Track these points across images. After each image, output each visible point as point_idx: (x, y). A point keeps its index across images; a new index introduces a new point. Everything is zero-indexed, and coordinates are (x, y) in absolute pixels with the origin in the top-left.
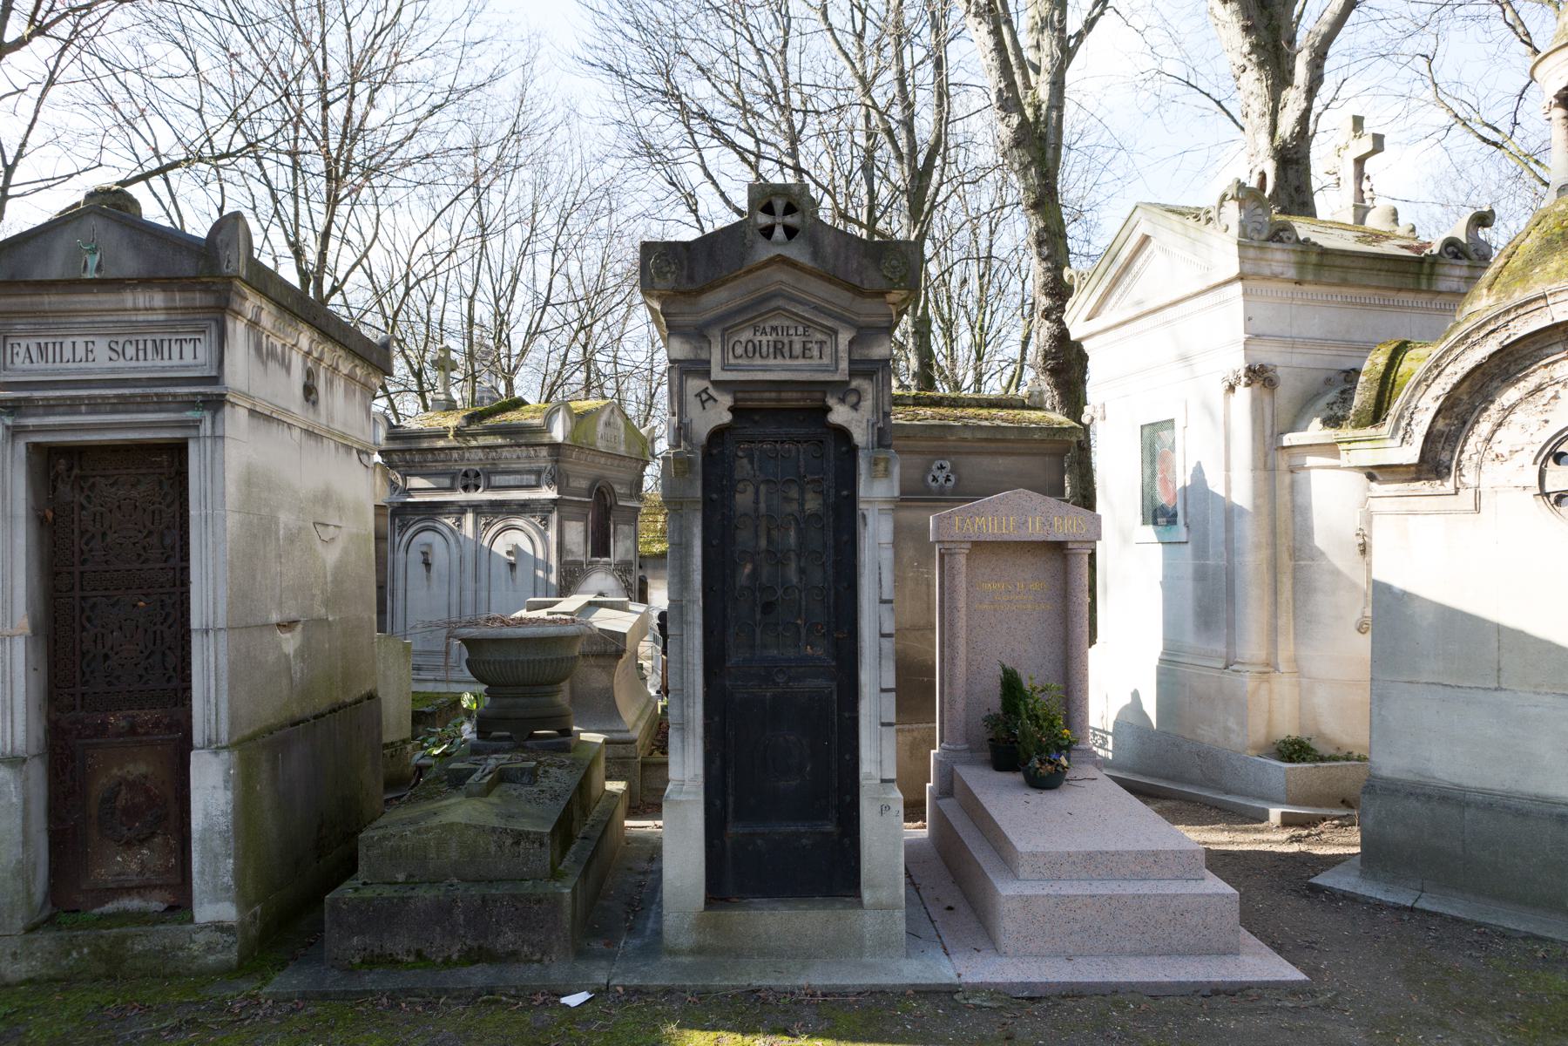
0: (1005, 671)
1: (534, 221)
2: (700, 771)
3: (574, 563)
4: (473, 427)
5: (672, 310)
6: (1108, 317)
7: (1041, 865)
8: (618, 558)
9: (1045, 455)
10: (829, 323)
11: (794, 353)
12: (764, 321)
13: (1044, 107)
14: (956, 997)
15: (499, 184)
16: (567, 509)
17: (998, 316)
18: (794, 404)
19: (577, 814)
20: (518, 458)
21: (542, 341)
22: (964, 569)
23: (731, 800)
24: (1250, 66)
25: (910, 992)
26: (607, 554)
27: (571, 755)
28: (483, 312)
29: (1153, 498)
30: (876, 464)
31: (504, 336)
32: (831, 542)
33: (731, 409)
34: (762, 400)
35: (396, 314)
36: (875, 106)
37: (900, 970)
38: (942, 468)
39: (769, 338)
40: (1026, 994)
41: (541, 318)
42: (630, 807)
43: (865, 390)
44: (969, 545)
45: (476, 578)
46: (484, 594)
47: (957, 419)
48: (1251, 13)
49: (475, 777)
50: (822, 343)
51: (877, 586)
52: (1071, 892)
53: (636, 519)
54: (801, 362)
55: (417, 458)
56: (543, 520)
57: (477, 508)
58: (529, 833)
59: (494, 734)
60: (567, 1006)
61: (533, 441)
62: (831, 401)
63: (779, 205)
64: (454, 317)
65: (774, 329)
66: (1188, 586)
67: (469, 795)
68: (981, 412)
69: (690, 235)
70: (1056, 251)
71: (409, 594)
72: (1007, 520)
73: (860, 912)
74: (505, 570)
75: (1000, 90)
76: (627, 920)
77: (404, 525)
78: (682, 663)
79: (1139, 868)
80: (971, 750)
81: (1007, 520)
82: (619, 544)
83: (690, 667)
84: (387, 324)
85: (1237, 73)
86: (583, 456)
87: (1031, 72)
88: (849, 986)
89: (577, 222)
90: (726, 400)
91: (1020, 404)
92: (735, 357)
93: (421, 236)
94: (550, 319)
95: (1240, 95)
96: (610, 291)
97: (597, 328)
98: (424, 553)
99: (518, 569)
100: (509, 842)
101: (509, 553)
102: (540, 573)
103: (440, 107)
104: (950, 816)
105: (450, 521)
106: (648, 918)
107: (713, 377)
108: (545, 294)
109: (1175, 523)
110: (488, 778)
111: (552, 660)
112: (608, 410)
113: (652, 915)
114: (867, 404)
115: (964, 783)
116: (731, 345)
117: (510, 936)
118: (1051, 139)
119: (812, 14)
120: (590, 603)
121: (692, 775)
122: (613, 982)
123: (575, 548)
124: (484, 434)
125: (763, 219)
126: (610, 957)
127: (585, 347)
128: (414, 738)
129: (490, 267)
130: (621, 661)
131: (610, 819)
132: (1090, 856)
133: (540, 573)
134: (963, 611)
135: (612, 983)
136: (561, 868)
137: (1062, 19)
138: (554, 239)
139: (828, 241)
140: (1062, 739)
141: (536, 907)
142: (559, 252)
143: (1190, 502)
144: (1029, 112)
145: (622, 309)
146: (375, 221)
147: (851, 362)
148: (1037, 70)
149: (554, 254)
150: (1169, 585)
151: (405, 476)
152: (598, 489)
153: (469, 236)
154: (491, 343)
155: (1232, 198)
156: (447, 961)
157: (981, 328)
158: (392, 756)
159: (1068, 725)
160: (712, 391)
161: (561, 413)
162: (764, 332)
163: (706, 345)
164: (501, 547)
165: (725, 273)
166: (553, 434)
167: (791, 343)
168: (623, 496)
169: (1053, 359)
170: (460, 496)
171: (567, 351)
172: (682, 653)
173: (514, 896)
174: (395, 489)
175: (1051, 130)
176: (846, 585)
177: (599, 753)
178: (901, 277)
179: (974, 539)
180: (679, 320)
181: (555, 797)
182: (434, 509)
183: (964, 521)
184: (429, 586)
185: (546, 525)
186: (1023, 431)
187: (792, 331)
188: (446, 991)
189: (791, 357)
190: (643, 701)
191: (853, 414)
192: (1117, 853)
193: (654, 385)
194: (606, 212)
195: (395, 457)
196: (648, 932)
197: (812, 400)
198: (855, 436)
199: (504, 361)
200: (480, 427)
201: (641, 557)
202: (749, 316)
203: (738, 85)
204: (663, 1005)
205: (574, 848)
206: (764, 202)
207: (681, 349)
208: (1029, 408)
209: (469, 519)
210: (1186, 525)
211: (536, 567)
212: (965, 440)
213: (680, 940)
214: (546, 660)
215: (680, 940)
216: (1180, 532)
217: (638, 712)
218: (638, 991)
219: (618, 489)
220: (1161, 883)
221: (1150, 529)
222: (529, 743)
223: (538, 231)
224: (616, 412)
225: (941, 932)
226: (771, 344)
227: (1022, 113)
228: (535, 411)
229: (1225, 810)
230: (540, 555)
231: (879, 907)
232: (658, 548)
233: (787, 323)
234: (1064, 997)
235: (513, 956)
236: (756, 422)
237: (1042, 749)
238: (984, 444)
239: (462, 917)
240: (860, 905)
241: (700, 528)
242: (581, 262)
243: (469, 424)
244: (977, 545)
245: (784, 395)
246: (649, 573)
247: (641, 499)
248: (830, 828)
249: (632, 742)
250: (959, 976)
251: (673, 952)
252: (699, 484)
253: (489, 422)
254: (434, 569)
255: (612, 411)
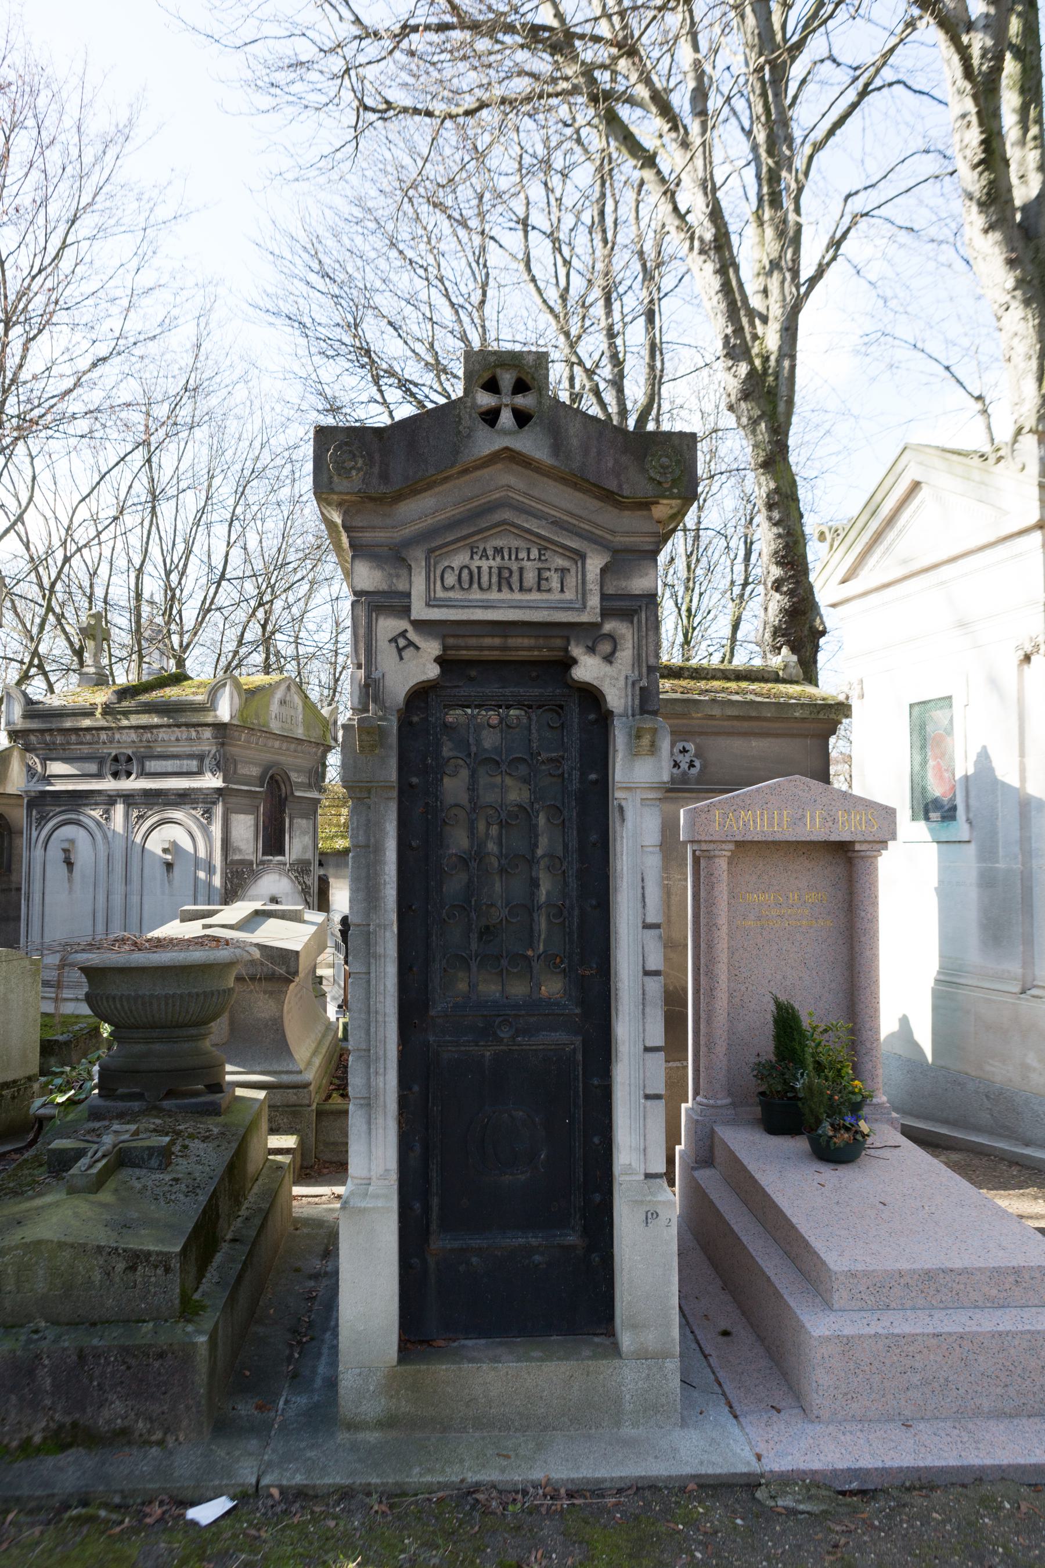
0: (779, 1005)
1: (210, 486)
2: (393, 1164)
3: (242, 862)
4: (125, 704)
5: (358, 522)
6: (869, 576)
7: (862, 1288)
8: (294, 857)
9: (806, 736)
10: (574, 544)
11: (526, 584)
12: (485, 539)
13: (773, 358)
14: (758, 1494)
15: (172, 446)
16: (233, 800)
17: (706, 598)
18: (523, 655)
19: (224, 1205)
20: (177, 740)
21: (215, 617)
22: (725, 876)
23: (435, 1201)
24: (1014, 304)
25: (692, 1486)
26: (281, 852)
27: (220, 1119)
28: (153, 587)
29: (924, 790)
30: (638, 737)
31: (174, 612)
32: (573, 844)
33: (439, 660)
34: (481, 648)
35: (53, 585)
36: (581, 363)
37: (675, 1450)
38: (684, 751)
39: (492, 563)
40: (854, 1485)
41: (216, 593)
42: (302, 1167)
43: (623, 636)
44: (732, 847)
45: (127, 880)
46: (135, 899)
47: (702, 692)
48: (1016, 244)
49: (84, 1162)
50: (563, 571)
51: (640, 905)
52: (907, 1329)
53: (315, 812)
54: (535, 596)
55: (59, 739)
56: (205, 812)
57: (129, 799)
58: (149, 1254)
59: (120, 1091)
60: (194, 1523)
61: (194, 720)
62: (576, 651)
63: (507, 380)
64: (120, 592)
65: (498, 551)
66: (972, 894)
67: (72, 1191)
68: (728, 685)
69: (383, 420)
70: (788, 515)
71: (47, 898)
72: (780, 814)
73: (616, 1362)
74: (160, 871)
75: (726, 336)
76: (289, 1359)
77: (42, 818)
78: (369, 1012)
79: (994, 1292)
80: (734, 1105)
81: (780, 814)
82: (295, 841)
83: (380, 1018)
84: (44, 596)
85: (1000, 312)
86: (254, 739)
87: (757, 321)
88: (604, 1480)
89: (256, 491)
90: (432, 648)
91: (773, 676)
92: (445, 588)
93: (84, 499)
94: (227, 595)
95: (1003, 336)
96: (291, 566)
97: (278, 604)
98: (65, 851)
99: (176, 869)
100: (121, 1266)
101: (165, 851)
102: (202, 875)
103: (104, 359)
104: (714, 1196)
105: (96, 813)
106: (319, 1355)
107: (414, 616)
108: (221, 567)
109: (953, 818)
110: (100, 1165)
111: (197, 995)
112: (283, 687)
113: (325, 1351)
114: (625, 655)
115: (722, 1140)
116: (438, 573)
117: (119, 1407)
118: (783, 390)
119: (514, 265)
120: (257, 913)
121: (381, 1171)
122: (264, 1482)
123: (243, 846)
124: (137, 712)
125: (485, 400)
126: (260, 1430)
127: (264, 627)
128: (42, 1073)
129: (161, 538)
130: (292, 986)
131: (272, 1205)
132: (929, 1276)
133: (202, 875)
134: (724, 929)
135: (264, 1482)
136: (196, 1296)
137: (796, 260)
138: (231, 510)
139: (573, 429)
140: (853, 1093)
141: (157, 1364)
142: (235, 522)
143: (972, 794)
144: (757, 362)
145: (305, 587)
146: (30, 484)
147: (604, 597)
148: (765, 320)
149: (230, 525)
150: (946, 892)
151: (44, 760)
152: (272, 777)
153: (136, 501)
154: (159, 620)
155: (1031, 431)
156: (26, 1448)
157: (689, 610)
158: (13, 1098)
159: (857, 1074)
160: (412, 635)
161: (227, 688)
162: (484, 555)
163: (404, 572)
164: (156, 844)
165: (432, 471)
166: (218, 713)
167: (521, 570)
168: (301, 786)
169: (783, 636)
170: (108, 784)
171: (244, 629)
172: (368, 999)
173: (125, 1350)
174: (33, 776)
175: (782, 380)
176: (594, 902)
177: (259, 1115)
178: (674, 481)
179: (739, 838)
180: (368, 536)
181: (193, 1190)
182: (78, 799)
183: (725, 815)
184: (71, 890)
185: (209, 819)
186: (782, 708)
187: (523, 555)
188: (18, 1500)
189: (521, 589)
190: (320, 1028)
191: (606, 669)
192: (964, 1272)
193: (339, 669)
194: (288, 481)
195: (33, 738)
196: (318, 1382)
197: (550, 649)
198: (609, 698)
199: (175, 639)
200: (133, 703)
201: (322, 854)
202: (464, 532)
203: (432, 345)
204: (335, 1517)
205: (218, 1258)
206: (486, 376)
207: (368, 577)
208: (784, 681)
209: (119, 809)
210: (969, 821)
211: (197, 867)
212: (712, 717)
213: (363, 1408)
214: (189, 994)
215: (363, 1408)
216: (961, 829)
217: (314, 1046)
218: (302, 1495)
219: (294, 777)
220: (1026, 1313)
221: (922, 825)
222: (166, 1104)
223: (215, 501)
224: (293, 689)
225: (721, 1374)
226: (495, 571)
227: (751, 362)
228: (199, 687)
229: (1028, 1168)
230: (202, 854)
231: (642, 1355)
232: (341, 844)
233: (515, 543)
234: (909, 1489)
235: (122, 1436)
236: (471, 679)
237: (833, 1110)
238: (735, 723)
239: (49, 1381)
240: (615, 1351)
241: (394, 823)
242: (261, 534)
243: (119, 701)
244: (742, 846)
245: (512, 642)
246: (331, 872)
247: (322, 790)
248: (572, 1239)
249: (306, 1086)
250: (759, 1457)
251: (352, 1426)
252: (393, 763)
253: (145, 698)
254: (77, 869)
255: (289, 688)
